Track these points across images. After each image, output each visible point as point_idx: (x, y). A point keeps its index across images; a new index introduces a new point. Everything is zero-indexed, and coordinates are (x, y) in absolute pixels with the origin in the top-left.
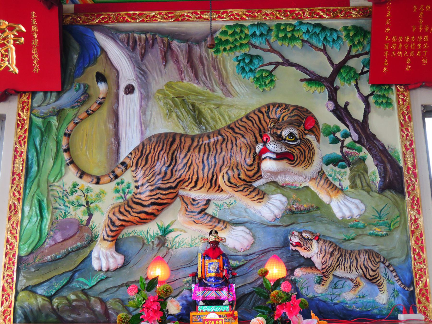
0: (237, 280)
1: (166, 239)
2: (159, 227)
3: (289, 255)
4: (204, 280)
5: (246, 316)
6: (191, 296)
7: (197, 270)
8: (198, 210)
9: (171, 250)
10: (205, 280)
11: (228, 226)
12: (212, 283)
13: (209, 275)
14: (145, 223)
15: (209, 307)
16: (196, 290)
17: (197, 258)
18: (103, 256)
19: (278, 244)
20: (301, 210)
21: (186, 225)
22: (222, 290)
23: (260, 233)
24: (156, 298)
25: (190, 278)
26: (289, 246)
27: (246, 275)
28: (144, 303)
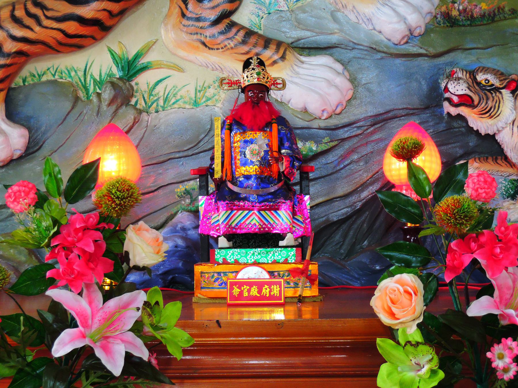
0: (314, 188)
1: (132, 87)
2: (114, 59)
3: (442, 127)
4: (229, 185)
5: (332, 275)
6: (197, 227)
7: (212, 159)
8: (213, 16)
9: (144, 114)
10: (234, 183)
11: (289, 55)
12: (250, 190)
13: (243, 170)
14: (80, 47)
15: (243, 250)
16: (210, 211)
17: (211, 133)
19: (415, 102)
20: (472, 16)
21: (182, 53)
22: (276, 210)
23: (369, 76)
24: (93, 220)
25: (194, 184)
26: (441, 106)
27: (332, 177)
28: (55, 234)
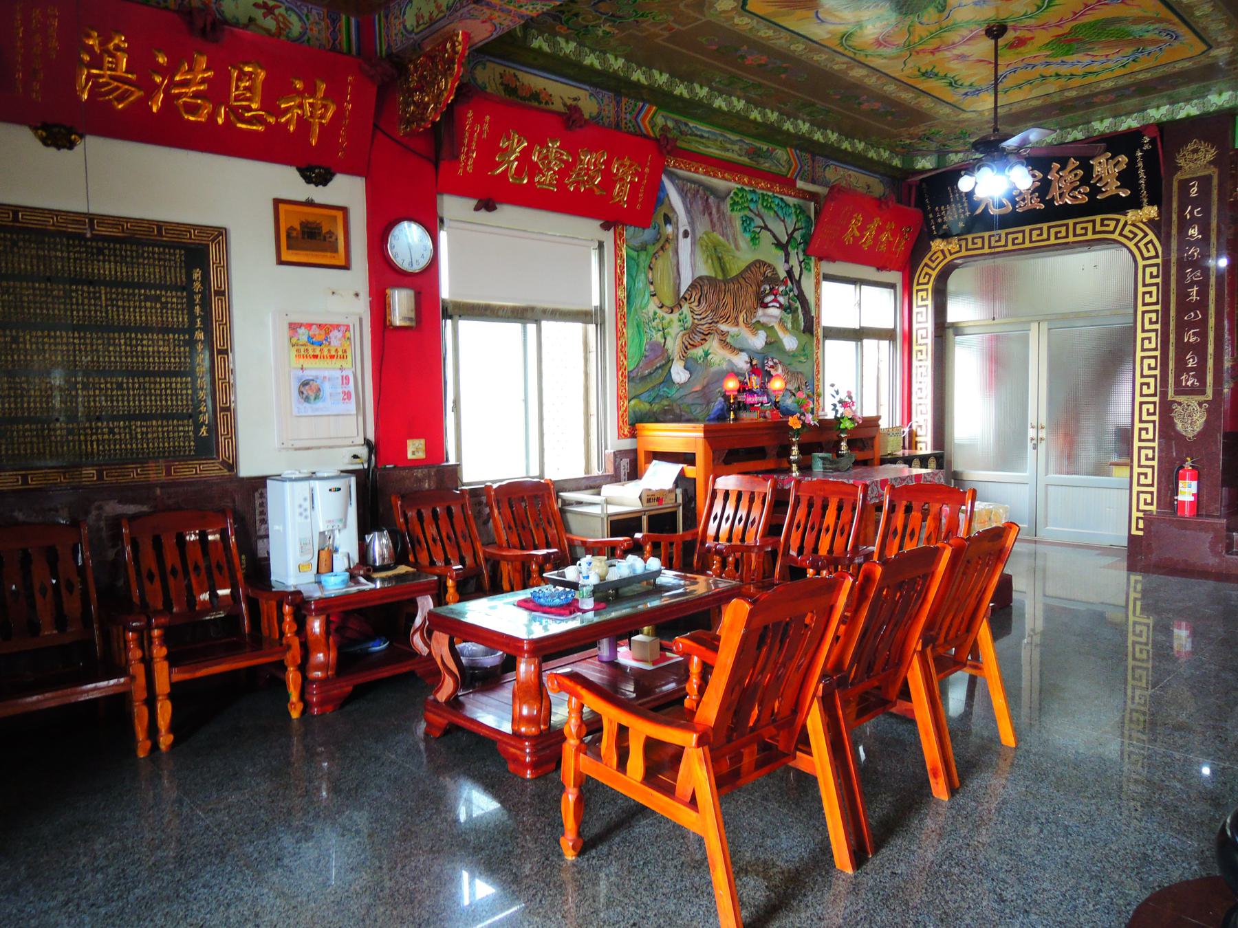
18: (679, 374)
